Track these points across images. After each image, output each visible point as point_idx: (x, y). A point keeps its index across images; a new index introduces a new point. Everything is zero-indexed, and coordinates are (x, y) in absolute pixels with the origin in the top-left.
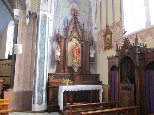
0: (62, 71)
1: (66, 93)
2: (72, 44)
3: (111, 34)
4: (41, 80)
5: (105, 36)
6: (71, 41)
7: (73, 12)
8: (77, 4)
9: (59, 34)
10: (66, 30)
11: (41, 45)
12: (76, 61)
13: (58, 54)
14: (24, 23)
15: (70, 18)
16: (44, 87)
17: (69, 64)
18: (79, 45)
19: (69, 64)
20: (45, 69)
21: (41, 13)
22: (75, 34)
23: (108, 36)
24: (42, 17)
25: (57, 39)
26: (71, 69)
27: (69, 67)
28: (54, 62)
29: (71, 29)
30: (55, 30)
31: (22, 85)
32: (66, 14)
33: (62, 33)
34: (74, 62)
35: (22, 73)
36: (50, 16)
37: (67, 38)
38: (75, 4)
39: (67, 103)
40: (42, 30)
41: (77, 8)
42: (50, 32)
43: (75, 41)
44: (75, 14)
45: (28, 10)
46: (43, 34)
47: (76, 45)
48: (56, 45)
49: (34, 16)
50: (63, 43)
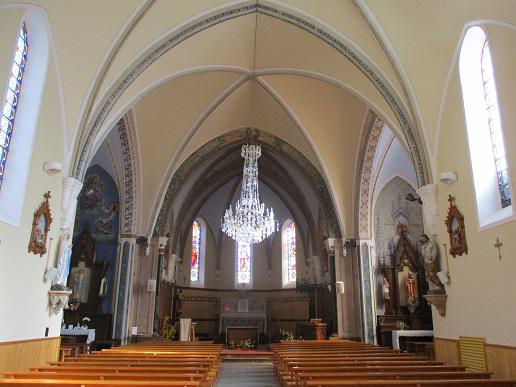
0: (394, 312)
1: (402, 339)
2: (404, 274)
3: (461, 219)
4: (370, 323)
5: (449, 223)
6: (402, 270)
7: (400, 230)
8: (405, 216)
9: (384, 265)
10: (393, 257)
11: (366, 281)
12: (410, 299)
13: (386, 290)
14: (341, 254)
15: (396, 239)
16: (375, 333)
17: (402, 301)
18: (414, 275)
19: (402, 301)
20: (373, 312)
21: (361, 242)
22: (406, 261)
23: (455, 226)
24: (363, 247)
25: (381, 270)
26: (405, 309)
27: (402, 307)
28: (381, 300)
29: (399, 255)
30: (378, 259)
31: (347, 329)
32: (391, 235)
33: (388, 262)
34: (409, 298)
35: (345, 315)
36: (371, 243)
37: (396, 267)
38: (401, 218)
39: (101, 292)
40: (364, 263)
41: (406, 223)
42: (373, 263)
43: (406, 271)
44: (402, 232)
45: (344, 239)
46: (367, 268)
47: (410, 277)
48: (382, 279)
49: (352, 245)
50: (390, 275)
